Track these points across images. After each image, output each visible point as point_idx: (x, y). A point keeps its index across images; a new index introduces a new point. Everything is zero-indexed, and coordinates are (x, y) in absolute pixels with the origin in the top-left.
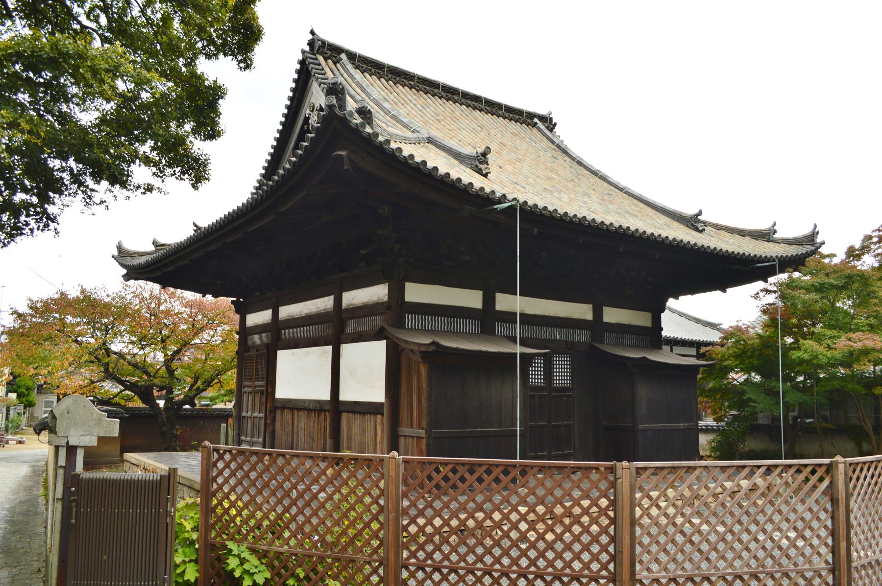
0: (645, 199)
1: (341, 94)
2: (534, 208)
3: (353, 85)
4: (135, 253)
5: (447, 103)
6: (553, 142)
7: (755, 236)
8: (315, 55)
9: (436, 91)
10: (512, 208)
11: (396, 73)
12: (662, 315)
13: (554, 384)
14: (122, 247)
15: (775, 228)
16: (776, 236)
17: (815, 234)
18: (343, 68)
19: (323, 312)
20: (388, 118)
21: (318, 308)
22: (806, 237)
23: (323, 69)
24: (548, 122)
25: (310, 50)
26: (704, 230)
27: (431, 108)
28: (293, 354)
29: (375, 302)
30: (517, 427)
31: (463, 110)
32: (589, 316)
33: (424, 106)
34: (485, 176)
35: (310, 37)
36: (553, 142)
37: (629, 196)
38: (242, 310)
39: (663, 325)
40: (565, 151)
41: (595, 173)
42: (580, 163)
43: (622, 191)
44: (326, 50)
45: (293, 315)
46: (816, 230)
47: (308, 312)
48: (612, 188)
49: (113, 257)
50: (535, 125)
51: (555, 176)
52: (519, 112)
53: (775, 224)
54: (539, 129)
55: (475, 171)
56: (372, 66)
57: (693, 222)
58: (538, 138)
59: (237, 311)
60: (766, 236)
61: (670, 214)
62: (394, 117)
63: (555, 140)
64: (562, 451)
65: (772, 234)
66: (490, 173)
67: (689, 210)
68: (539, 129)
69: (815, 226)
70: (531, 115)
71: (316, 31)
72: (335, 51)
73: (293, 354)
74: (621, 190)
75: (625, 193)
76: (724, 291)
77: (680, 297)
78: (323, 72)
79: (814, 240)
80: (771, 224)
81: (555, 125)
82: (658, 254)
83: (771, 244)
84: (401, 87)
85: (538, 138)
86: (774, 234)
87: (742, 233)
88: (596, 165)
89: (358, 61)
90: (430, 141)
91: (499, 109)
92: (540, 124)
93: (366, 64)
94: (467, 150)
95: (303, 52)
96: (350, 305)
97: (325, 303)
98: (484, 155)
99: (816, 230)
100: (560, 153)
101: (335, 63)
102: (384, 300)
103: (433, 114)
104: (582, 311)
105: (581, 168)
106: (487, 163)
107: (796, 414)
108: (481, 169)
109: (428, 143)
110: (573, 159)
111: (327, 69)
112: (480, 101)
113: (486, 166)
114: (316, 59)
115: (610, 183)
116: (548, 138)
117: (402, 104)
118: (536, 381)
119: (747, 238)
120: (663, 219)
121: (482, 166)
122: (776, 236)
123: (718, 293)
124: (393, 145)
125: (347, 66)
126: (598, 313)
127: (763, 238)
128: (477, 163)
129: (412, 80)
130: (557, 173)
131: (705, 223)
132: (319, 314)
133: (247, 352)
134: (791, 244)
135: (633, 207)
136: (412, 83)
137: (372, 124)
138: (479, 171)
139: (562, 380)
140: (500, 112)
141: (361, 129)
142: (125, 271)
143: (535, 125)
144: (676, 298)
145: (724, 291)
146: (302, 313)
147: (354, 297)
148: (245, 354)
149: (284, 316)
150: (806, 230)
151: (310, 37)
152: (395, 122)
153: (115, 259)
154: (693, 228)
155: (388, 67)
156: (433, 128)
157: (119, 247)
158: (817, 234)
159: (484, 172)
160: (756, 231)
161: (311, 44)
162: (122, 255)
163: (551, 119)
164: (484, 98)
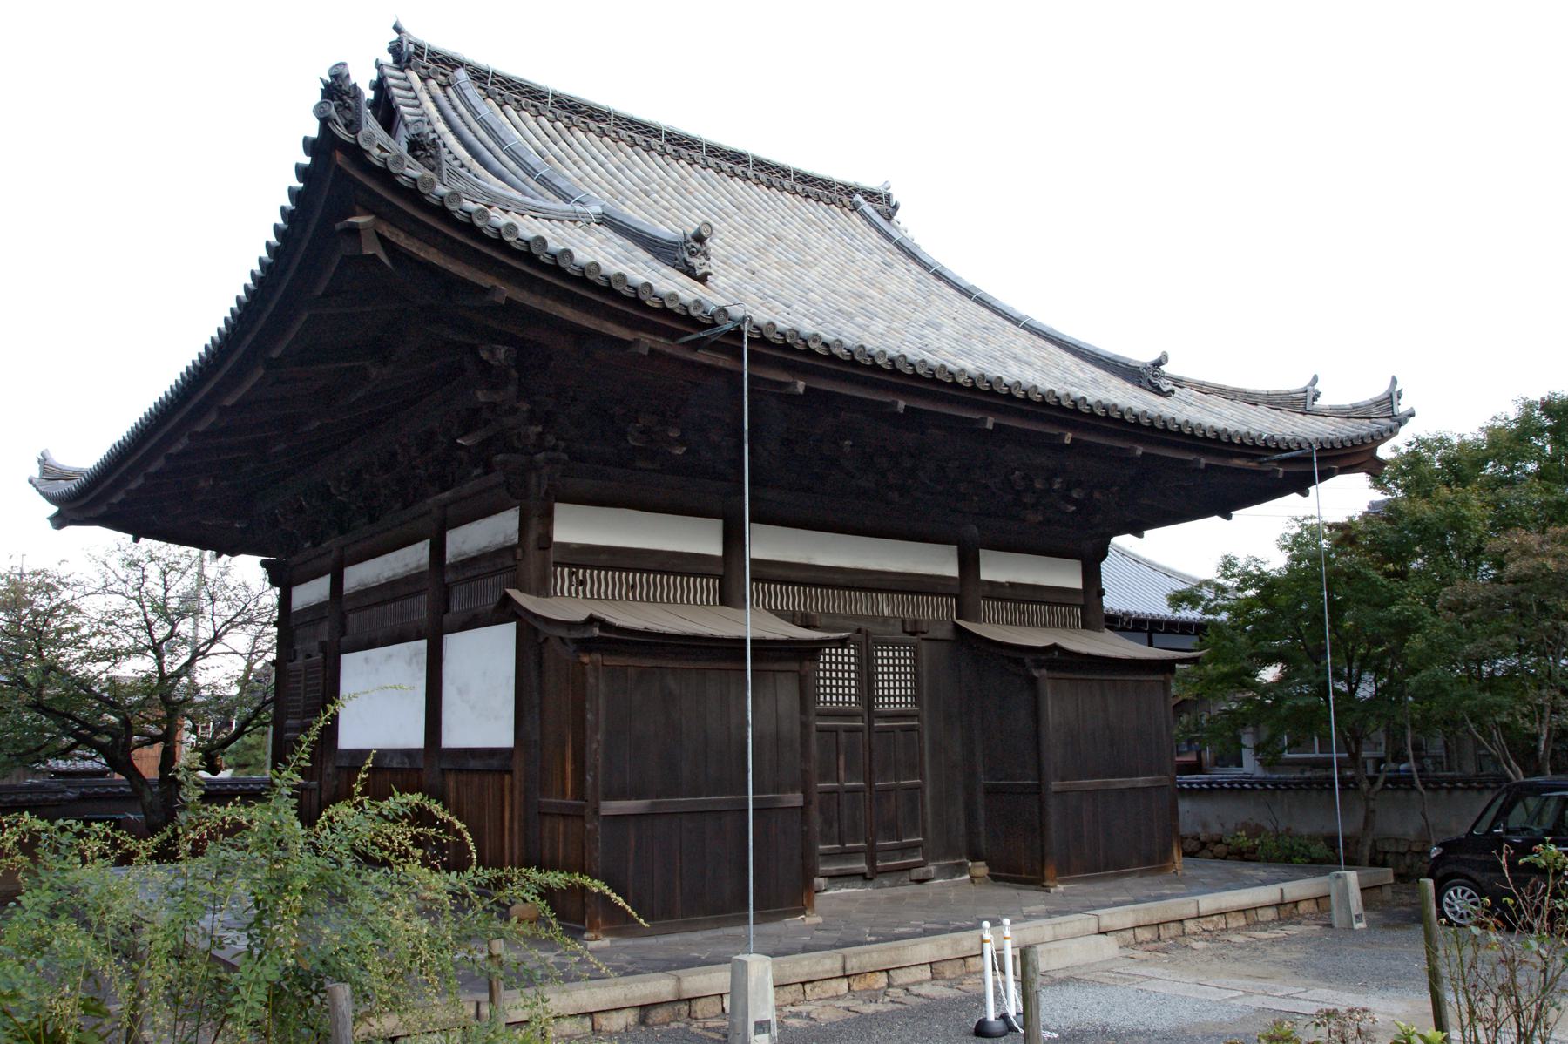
0: (1060, 337)
1: (352, 98)
2: (791, 337)
3: (475, 126)
4: (74, 472)
5: (674, 163)
6: (889, 237)
7: (1278, 404)
8: (402, 71)
9: (654, 142)
10: (737, 334)
11: (571, 107)
12: (1104, 565)
13: (878, 704)
14: (49, 462)
15: (1316, 387)
16: (1322, 402)
17: (1395, 398)
18: (458, 95)
19: (414, 572)
20: (532, 182)
21: (406, 565)
22: (1377, 403)
23: (416, 98)
24: (884, 203)
25: (395, 62)
26: (1172, 391)
27: (638, 171)
28: (367, 660)
29: (499, 547)
30: (753, 799)
31: (707, 176)
32: (952, 570)
33: (623, 167)
34: (703, 279)
35: (395, 36)
36: (889, 237)
37: (1030, 332)
38: (280, 576)
39: (1106, 582)
40: (912, 255)
41: (966, 292)
42: (939, 275)
43: (1017, 325)
44: (425, 62)
45: (366, 582)
46: (1397, 389)
47: (391, 574)
48: (999, 319)
49: (31, 482)
50: (855, 207)
51: (873, 292)
52: (826, 184)
53: (1315, 380)
54: (864, 215)
55: (681, 271)
56: (521, 93)
57: (1147, 377)
58: (859, 231)
59: (274, 582)
60: (1300, 402)
61: (1108, 364)
62: (544, 181)
63: (893, 232)
64: (899, 839)
65: (1309, 400)
66: (710, 274)
67: (1142, 355)
68: (864, 215)
69: (1394, 381)
70: (849, 190)
71: (405, 26)
72: (443, 62)
73: (367, 660)
74: (1016, 321)
75: (1023, 328)
76: (1228, 516)
77: (1146, 533)
78: (416, 102)
79: (1392, 409)
80: (1309, 379)
81: (896, 207)
82: (1070, 435)
83: (1308, 418)
84: (580, 134)
85: (859, 231)
86: (1314, 399)
87: (1251, 399)
88: (968, 278)
89: (492, 83)
90: (606, 220)
91: (784, 176)
92: (867, 207)
93: (508, 88)
94: (666, 230)
95: (379, 66)
96: (460, 555)
97: (415, 556)
98: (699, 238)
99: (1397, 389)
100: (902, 257)
101: (443, 87)
102: (513, 542)
103: (637, 181)
104: (940, 563)
105: (941, 284)
106: (705, 254)
107: (1381, 752)
108: (693, 268)
109: (599, 224)
110: (926, 266)
111: (425, 97)
112: (745, 162)
113: (703, 260)
114: (406, 79)
115: (995, 310)
116: (879, 230)
117: (575, 163)
118: (841, 698)
119: (1262, 408)
120: (1022, 342)
121: (695, 261)
122: (1322, 402)
123: (1216, 520)
124: (499, 218)
125: (466, 92)
126: (969, 564)
127: (1294, 406)
128: (686, 255)
129: (604, 121)
130: (882, 289)
131: (1178, 382)
132: (407, 577)
133: (291, 661)
134: (1348, 418)
135: (1032, 351)
136: (603, 125)
137: (440, 169)
138: (690, 272)
139: (837, 694)
140: (787, 184)
141: (394, 170)
142: (54, 509)
143: (855, 207)
144: (1138, 533)
145: (1228, 516)
146: (381, 577)
147: (466, 540)
148: (290, 665)
149: (352, 586)
150: (1378, 390)
151: (395, 36)
152: (544, 190)
153: (34, 486)
154: (1150, 388)
155: (554, 96)
156: (628, 203)
157: (44, 463)
158: (1399, 397)
159: (699, 272)
160: (1278, 394)
161: (396, 50)
162: (49, 472)
163: (888, 197)
164: (753, 157)
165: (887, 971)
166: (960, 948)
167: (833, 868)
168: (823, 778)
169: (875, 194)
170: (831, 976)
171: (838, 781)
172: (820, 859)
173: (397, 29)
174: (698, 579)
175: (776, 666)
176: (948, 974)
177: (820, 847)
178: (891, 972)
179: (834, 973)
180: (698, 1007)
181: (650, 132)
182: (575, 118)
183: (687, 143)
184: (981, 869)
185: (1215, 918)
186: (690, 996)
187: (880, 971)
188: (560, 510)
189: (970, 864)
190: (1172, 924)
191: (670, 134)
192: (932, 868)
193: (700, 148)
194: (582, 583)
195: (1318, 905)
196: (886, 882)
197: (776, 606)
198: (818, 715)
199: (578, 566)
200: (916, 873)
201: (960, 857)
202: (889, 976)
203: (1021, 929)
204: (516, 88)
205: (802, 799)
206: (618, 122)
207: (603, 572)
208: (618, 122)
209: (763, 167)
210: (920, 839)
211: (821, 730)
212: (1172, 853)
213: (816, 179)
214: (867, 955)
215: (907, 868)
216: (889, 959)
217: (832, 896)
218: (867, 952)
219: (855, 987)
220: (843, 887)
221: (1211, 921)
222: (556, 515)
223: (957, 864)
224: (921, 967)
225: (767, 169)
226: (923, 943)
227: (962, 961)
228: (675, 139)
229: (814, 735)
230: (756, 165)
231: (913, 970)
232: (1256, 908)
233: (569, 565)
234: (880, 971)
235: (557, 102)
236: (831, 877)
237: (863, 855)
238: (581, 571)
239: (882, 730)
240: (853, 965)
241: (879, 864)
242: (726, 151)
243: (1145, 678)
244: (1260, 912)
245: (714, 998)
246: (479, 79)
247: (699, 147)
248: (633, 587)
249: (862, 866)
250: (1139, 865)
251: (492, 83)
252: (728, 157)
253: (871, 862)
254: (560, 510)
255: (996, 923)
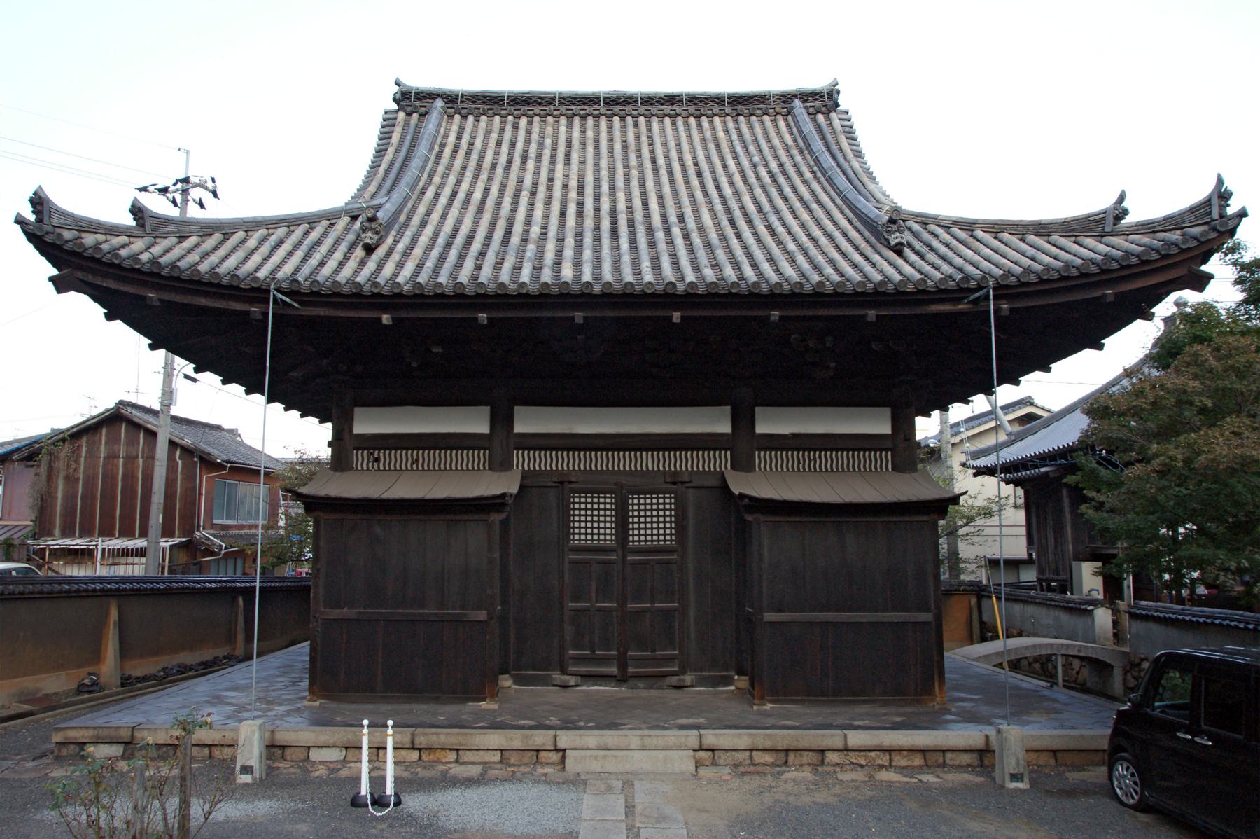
89: (462, 102)
151: (396, 88)
165: (458, 750)
166: (531, 742)
167: (583, 669)
168: (576, 598)
169: (816, 94)
170: (400, 746)
171: (590, 602)
172: (571, 661)
173: (397, 83)
174: (834, 453)
175: (466, 517)
176: (512, 761)
177: (571, 652)
178: (461, 752)
179: (403, 744)
180: (288, 752)
181: (591, 101)
182: (739, 107)
183: (624, 101)
184: (742, 682)
185: (873, 754)
186: (285, 744)
187: (450, 749)
188: (519, 411)
189: (736, 677)
190: (806, 753)
191: (418, 94)
192: (688, 678)
193: (681, 101)
194: (377, 460)
195: (925, 759)
196: (641, 685)
197: (715, 467)
198: (570, 550)
199: (374, 449)
200: (674, 680)
201: (727, 670)
202: (458, 755)
203: (602, 735)
204: (479, 99)
205: (486, 616)
206: (563, 101)
207: (884, 453)
208: (563, 101)
209: (696, 101)
210: (677, 652)
211: (572, 562)
212: (934, 688)
213: (751, 97)
214: (435, 736)
215: (664, 675)
216: (456, 741)
217: (582, 691)
218: (650, 736)
219: (424, 757)
220: (596, 685)
221: (866, 757)
222: (757, 416)
223: (722, 676)
224: (491, 752)
225: (701, 101)
226: (494, 733)
227: (535, 753)
228: (613, 101)
229: (567, 565)
230: (690, 101)
231: (481, 753)
232: (944, 751)
233: (367, 448)
234: (450, 749)
235: (512, 101)
236: (582, 676)
237: (615, 661)
238: (377, 452)
239: (634, 564)
240: (421, 741)
241: (630, 670)
242: (661, 98)
243: (901, 519)
244: (949, 755)
245: (301, 749)
246: (452, 102)
247: (635, 101)
248: (417, 460)
249: (614, 670)
250: (885, 693)
251: (462, 102)
252: (663, 101)
253: (623, 666)
254: (519, 411)
255: (378, 725)
